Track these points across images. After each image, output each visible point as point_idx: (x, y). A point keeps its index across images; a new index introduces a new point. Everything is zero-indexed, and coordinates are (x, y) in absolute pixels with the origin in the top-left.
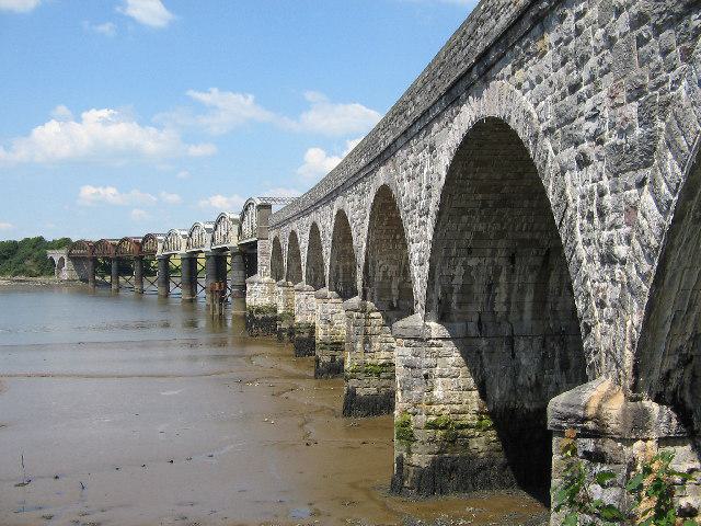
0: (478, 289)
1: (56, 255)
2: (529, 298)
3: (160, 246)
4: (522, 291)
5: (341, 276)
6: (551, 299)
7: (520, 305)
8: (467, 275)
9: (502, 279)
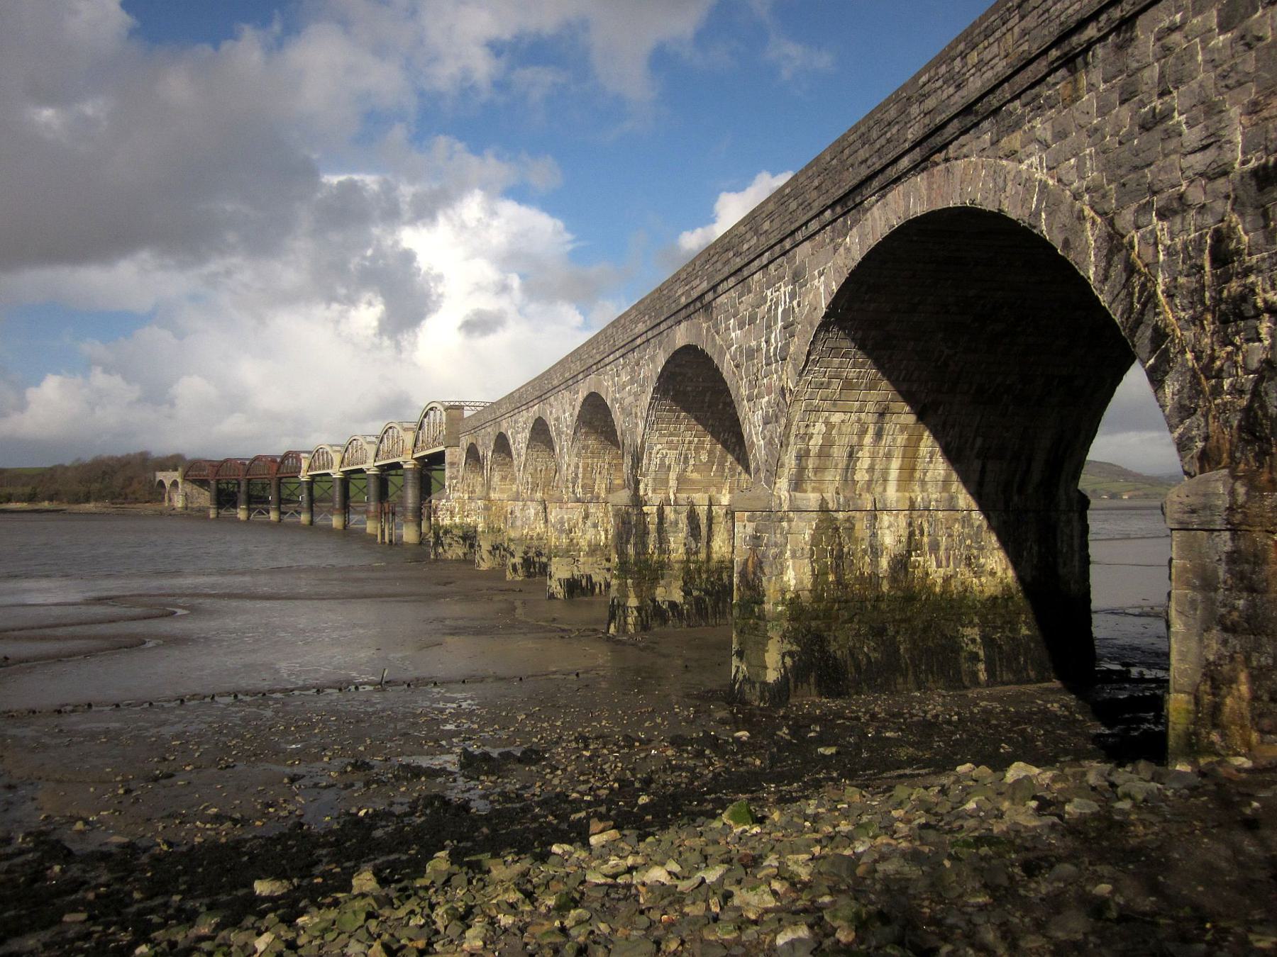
0: (839, 453)
1: (167, 477)
2: (895, 464)
3: (305, 465)
4: (888, 456)
5: (580, 476)
6: (920, 466)
7: (885, 473)
8: (827, 436)
9: (868, 439)
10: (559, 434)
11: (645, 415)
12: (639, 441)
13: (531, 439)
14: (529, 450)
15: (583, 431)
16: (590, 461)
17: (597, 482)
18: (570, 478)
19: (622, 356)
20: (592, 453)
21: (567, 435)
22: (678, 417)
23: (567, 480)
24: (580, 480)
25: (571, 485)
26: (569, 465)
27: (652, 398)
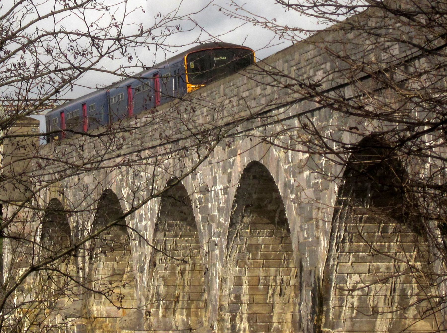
5: (245, 299)
10: (208, 219)
11: (328, 226)
12: (321, 270)
13: (162, 212)
14: (160, 235)
15: (247, 220)
16: (261, 273)
17: (277, 310)
18: (226, 303)
19: (298, 116)
20: (265, 257)
21: (219, 225)
22: (385, 230)
23: (221, 308)
24: (244, 308)
25: (228, 317)
26: (223, 281)
27: (339, 202)
